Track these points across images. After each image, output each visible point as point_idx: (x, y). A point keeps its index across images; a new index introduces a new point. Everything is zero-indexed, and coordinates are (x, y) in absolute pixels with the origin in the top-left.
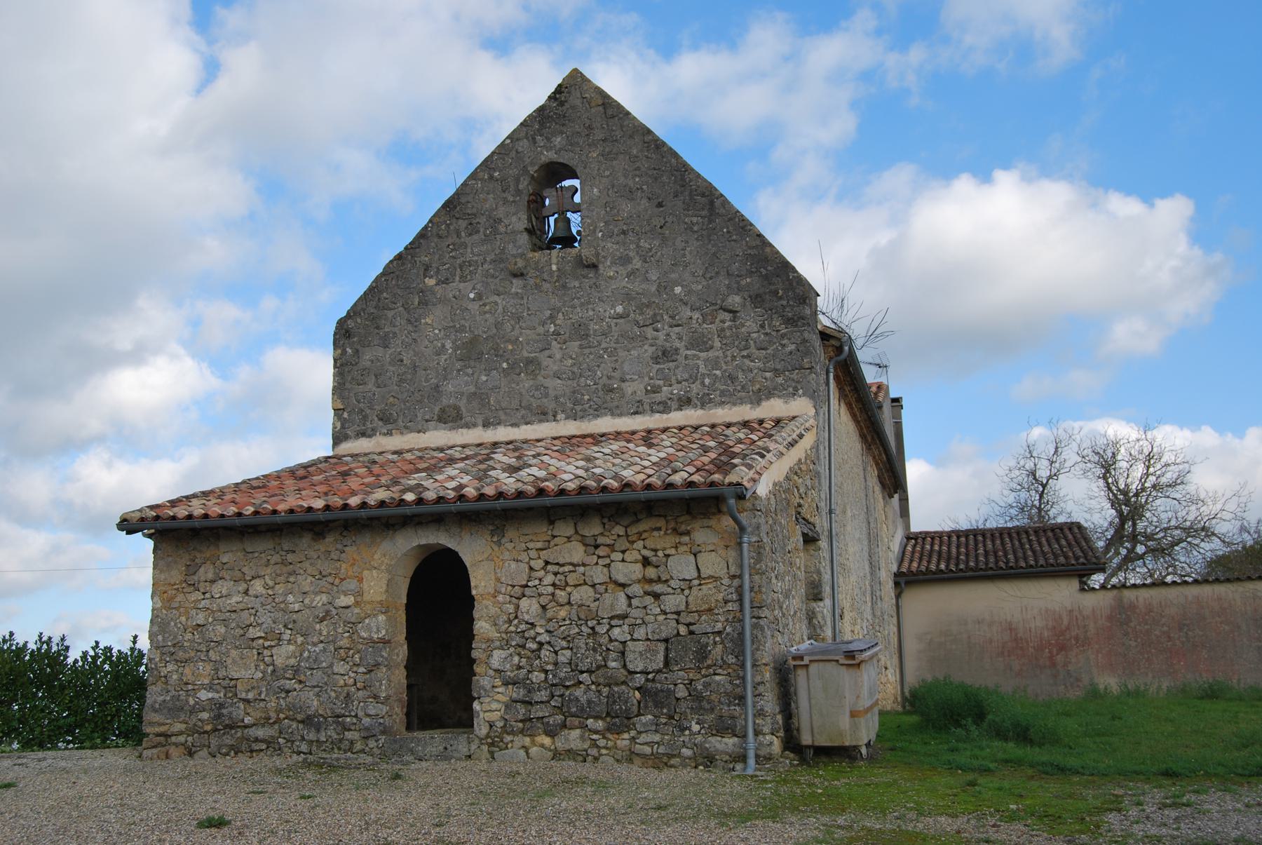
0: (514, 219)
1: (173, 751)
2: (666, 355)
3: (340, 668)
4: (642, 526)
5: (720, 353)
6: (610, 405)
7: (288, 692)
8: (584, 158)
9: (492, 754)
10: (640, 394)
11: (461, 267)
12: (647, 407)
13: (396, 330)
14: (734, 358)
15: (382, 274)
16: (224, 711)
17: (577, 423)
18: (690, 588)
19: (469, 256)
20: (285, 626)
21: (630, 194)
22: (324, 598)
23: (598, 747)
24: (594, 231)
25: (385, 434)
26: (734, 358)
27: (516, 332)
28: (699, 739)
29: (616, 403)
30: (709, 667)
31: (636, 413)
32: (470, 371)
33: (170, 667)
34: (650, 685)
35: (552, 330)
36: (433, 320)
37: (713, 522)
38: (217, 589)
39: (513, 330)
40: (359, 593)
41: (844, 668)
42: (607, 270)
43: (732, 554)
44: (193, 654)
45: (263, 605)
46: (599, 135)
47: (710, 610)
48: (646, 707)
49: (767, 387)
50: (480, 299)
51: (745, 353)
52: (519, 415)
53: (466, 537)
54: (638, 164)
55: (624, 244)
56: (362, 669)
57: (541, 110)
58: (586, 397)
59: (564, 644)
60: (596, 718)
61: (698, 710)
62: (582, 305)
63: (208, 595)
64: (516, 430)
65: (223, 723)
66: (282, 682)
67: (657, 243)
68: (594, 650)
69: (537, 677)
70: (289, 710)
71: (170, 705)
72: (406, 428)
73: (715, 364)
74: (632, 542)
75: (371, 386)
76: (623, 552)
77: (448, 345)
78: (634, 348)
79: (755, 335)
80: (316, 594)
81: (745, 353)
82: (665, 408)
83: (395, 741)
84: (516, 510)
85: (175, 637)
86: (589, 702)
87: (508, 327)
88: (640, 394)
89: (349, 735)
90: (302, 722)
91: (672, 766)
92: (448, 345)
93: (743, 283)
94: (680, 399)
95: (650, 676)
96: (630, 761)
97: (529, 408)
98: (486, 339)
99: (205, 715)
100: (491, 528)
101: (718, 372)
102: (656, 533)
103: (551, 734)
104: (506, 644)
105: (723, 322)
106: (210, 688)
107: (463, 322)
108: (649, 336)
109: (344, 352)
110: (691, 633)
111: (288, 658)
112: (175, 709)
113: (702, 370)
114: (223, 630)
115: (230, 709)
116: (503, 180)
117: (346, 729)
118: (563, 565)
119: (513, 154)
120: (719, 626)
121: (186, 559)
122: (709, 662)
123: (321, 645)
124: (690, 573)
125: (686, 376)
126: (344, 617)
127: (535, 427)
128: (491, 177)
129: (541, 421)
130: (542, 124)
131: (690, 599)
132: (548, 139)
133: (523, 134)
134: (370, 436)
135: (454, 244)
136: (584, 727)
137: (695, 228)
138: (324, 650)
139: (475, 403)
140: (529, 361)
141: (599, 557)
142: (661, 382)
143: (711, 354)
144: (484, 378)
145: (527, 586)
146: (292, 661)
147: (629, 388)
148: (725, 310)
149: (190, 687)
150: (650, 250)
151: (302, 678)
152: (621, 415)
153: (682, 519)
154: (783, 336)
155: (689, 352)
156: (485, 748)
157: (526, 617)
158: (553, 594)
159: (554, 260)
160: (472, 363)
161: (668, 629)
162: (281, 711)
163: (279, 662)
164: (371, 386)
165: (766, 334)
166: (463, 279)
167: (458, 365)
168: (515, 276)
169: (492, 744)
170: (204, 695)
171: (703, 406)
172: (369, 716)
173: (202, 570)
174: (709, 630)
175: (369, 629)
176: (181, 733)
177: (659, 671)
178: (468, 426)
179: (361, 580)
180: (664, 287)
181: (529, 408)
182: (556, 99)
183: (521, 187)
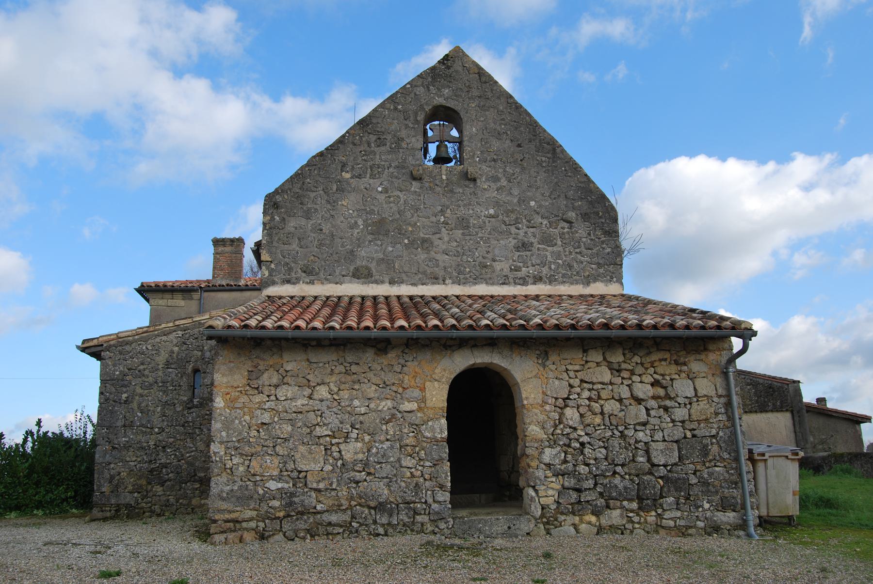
0: (413, 140)
1: (248, 536)
2: (524, 246)
3: (408, 462)
4: (655, 357)
5: (561, 249)
6: (485, 276)
7: (357, 482)
8: (465, 106)
9: (548, 532)
10: (506, 271)
11: (371, 168)
12: (511, 280)
13: (317, 207)
14: (570, 253)
15: (307, 165)
16: (296, 500)
17: (461, 287)
18: (690, 404)
19: (377, 161)
20: (353, 427)
21: (499, 135)
22: (389, 403)
23: (633, 522)
24: (473, 156)
25: (307, 283)
26: (570, 253)
27: (415, 219)
28: (708, 514)
29: (489, 276)
30: (710, 461)
31: (503, 284)
32: (379, 243)
33: (236, 460)
34: (670, 475)
35: (442, 220)
36: (348, 204)
37: (703, 357)
38: (282, 393)
39: (413, 216)
40: (424, 400)
41: (789, 461)
42: (483, 184)
43: (719, 381)
44: (259, 449)
45: (328, 407)
46: (475, 93)
47: (707, 420)
48: (669, 491)
49: (593, 275)
50: (387, 192)
51: (578, 250)
52: (417, 278)
53: (517, 359)
54: (503, 117)
55: (495, 168)
56: (428, 464)
57: (433, 69)
58: (468, 270)
59: (601, 444)
60: (630, 500)
61: (707, 493)
62: (465, 205)
63: (273, 398)
64: (415, 288)
65: (294, 510)
66: (352, 474)
67: (518, 170)
68: (626, 448)
69: (583, 469)
70: (361, 497)
71: (238, 494)
72: (326, 279)
73: (558, 256)
74: (646, 369)
75: (295, 246)
76: (640, 375)
77: (360, 222)
78: (502, 239)
79: (584, 240)
80: (382, 400)
81: (578, 250)
82: (524, 282)
83: (464, 523)
84: (555, 339)
85: (240, 434)
86: (625, 488)
87: (408, 214)
88: (506, 271)
89: (419, 518)
90: (375, 508)
91: (690, 535)
92: (360, 222)
93: (576, 204)
94: (534, 277)
95: (669, 468)
96: (657, 532)
97: (424, 273)
98: (392, 221)
99: (276, 503)
100: (538, 352)
101: (560, 261)
102: (663, 363)
103: (597, 513)
104: (553, 444)
105: (563, 228)
106: (279, 479)
107: (372, 207)
108: (513, 232)
109: (272, 219)
110: (694, 436)
111: (356, 453)
112: (244, 498)
113: (549, 258)
114: (290, 428)
115: (302, 498)
116: (404, 112)
117: (416, 513)
118: (593, 384)
119: (412, 95)
120: (714, 432)
121: (249, 365)
122: (711, 457)
123: (388, 443)
124: (690, 393)
125: (538, 262)
126: (408, 419)
127: (430, 287)
128: (396, 109)
129: (433, 283)
130: (434, 78)
131: (692, 411)
132: (439, 89)
133: (419, 83)
134: (294, 284)
135: (365, 151)
136: (622, 507)
137: (544, 164)
138: (392, 447)
139: (383, 266)
140: (424, 241)
141: (623, 378)
142: (521, 265)
143: (555, 249)
144: (391, 249)
145: (568, 398)
146: (360, 456)
147: (498, 266)
148: (564, 221)
149: (258, 478)
150: (514, 174)
151: (372, 471)
152: (493, 284)
153: (682, 353)
154: (603, 242)
155: (540, 246)
156: (541, 526)
157: (571, 423)
158: (589, 406)
159: (444, 172)
160: (381, 237)
161: (678, 433)
162: (352, 498)
163: (348, 456)
164: (295, 246)
165: (592, 240)
166: (372, 176)
167: (370, 237)
168: (414, 179)
169: (548, 523)
170: (273, 485)
171: (550, 283)
172: (439, 502)
173: (266, 375)
174: (707, 434)
175: (433, 430)
176: (251, 519)
177: (676, 464)
178: (376, 282)
179: (423, 390)
180: (522, 201)
181: (424, 273)
182: (444, 64)
183: (419, 118)
